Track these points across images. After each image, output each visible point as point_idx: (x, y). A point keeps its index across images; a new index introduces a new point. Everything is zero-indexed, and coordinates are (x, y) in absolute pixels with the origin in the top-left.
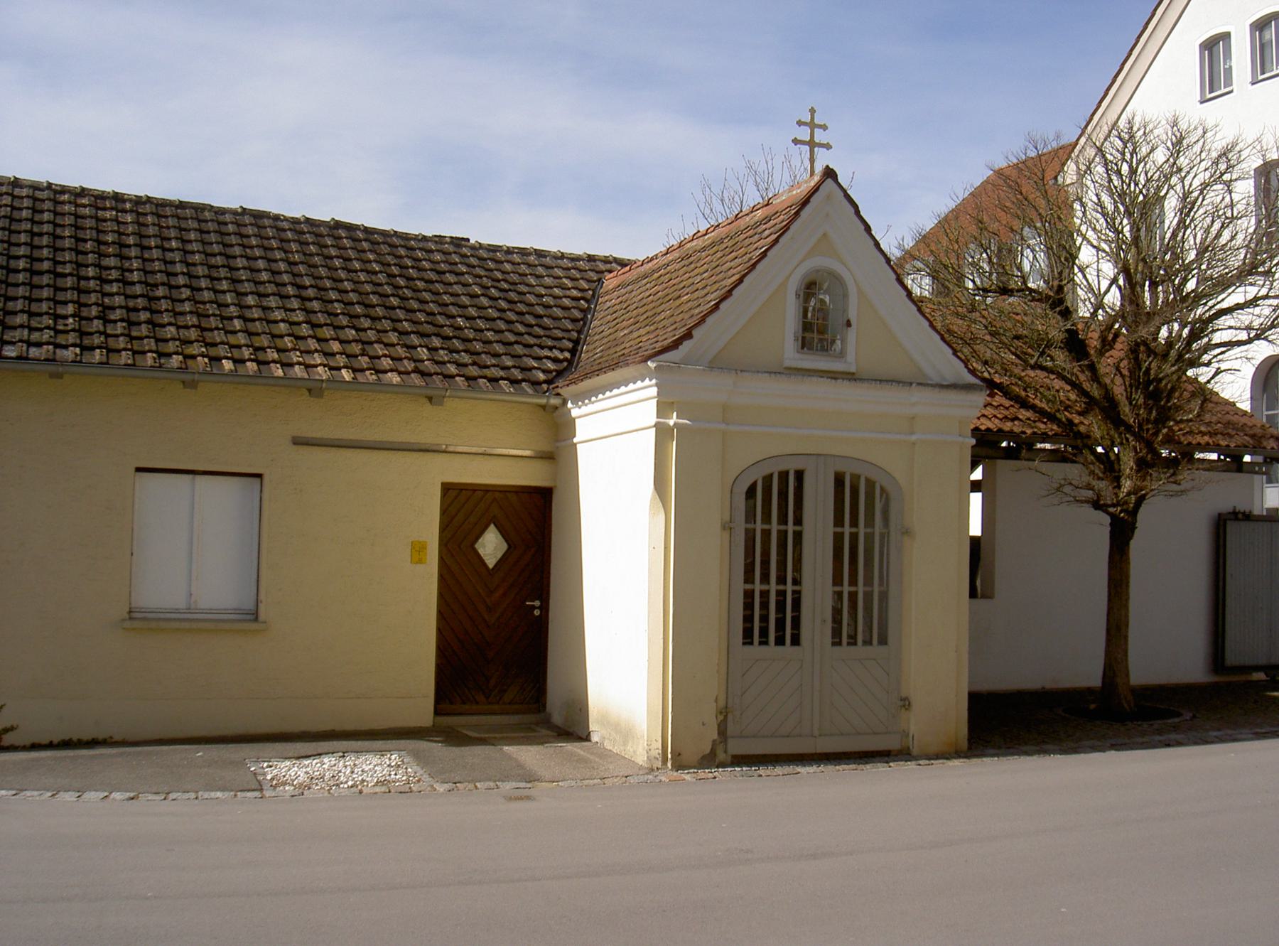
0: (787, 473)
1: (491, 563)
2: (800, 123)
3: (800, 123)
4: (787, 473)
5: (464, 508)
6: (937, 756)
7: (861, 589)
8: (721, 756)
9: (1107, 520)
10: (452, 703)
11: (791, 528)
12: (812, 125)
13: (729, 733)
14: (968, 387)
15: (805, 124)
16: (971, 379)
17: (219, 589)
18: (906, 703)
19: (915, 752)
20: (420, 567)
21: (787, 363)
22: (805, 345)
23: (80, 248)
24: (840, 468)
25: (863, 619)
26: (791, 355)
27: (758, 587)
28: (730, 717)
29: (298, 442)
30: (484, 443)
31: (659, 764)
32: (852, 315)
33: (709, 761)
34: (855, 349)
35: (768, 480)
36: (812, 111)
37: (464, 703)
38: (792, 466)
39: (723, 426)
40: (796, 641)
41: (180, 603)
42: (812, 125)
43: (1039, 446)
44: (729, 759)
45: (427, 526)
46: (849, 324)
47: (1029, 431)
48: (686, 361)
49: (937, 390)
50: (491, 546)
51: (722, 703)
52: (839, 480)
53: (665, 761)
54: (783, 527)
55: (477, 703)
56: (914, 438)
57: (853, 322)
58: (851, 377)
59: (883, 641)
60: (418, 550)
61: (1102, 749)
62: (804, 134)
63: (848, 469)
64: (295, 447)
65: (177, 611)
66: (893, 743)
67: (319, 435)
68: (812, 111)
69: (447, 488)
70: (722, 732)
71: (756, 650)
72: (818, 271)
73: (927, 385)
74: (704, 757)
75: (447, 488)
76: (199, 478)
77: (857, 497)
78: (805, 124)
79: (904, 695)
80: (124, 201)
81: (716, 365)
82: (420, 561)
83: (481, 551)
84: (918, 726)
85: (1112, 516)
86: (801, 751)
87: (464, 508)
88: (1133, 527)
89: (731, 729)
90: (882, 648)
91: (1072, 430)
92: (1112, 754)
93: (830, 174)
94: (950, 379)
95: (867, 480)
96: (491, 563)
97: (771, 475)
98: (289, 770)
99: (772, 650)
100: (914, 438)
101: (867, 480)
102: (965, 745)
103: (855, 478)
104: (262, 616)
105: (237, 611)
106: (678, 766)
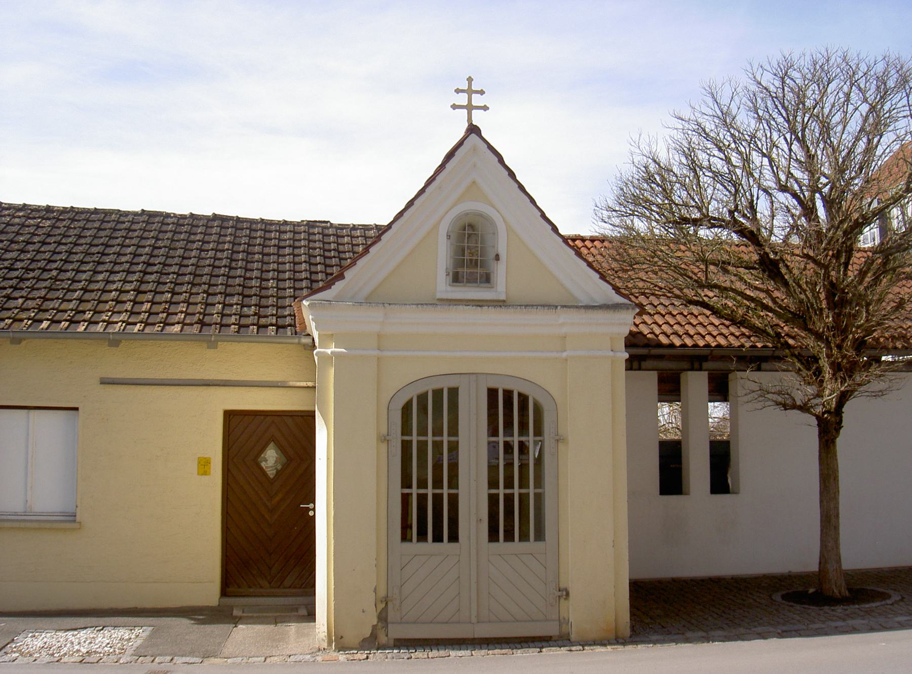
0: (441, 390)
1: (271, 473)
2: (458, 91)
3: (458, 91)
4: (441, 390)
5: (244, 432)
6: (603, 643)
7: (532, 491)
8: (383, 639)
9: (814, 421)
10: (239, 587)
11: (415, 438)
12: (470, 92)
13: (389, 619)
14: (616, 307)
15: (477, 92)
16: (619, 299)
17: (47, 498)
18: (565, 594)
19: (573, 637)
20: (205, 478)
21: (439, 296)
22: (456, 279)
23: (281, 253)
24: (493, 385)
25: (516, 516)
26: (443, 287)
27: (501, 491)
28: (390, 604)
29: (105, 382)
30: (254, 374)
31: (325, 645)
32: (502, 250)
33: (371, 643)
34: (504, 281)
35: (422, 398)
36: (470, 80)
37: (250, 587)
38: (445, 384)
39: (376, 353)
40: (454, 537)
41: (20, 508)
42: (470, 92)
43: (883, 358)
44: (392, 643)
45: (212, 444)
46: (497, 257)
47: (748, 345)
48: (339, 299)
49: (583, 311)
50: (271, 458)
51: (382, 593)
52: (492, 393)
53: (330, 644)
54: (523, 439)
55: (261, 587)
56: (565, 354)
57: (503, 256)
58: (500, 304)
59: (540, 535)
60: (204, 465)
61: (763, 636)
62: (463, 99)
63: (501, 386)
64: (102, 386)
65: (16, 514)
66: (551, 629)
67: (142, 376)
68: (470, 80)
69: (230, 416)
70: (383, 617)
71: (415, 547)
72: (467, 214)
73: (577, 307)
74: (364, 640)
75: (230, 416)
76: (32, 412)
77: (514, 412)
78: (477, 92)
79: (562, 586)
80: (53, 212)
81: (370, 301)
82: (205, 473)
83: (263, 464)
84: (577, 615)
85: (817, 417)
86: (488, 636)
87: (244, 432)
88: (839, 425)
89: (391, 615)
90: (453, 545)
91: (779, 342)
92: (774, 642)
93: (473, 130)
94: (600, 301)
95: (520, 394)
96: (271, 473)
97: (427, 393)
98: (40, 640)
99: (430, 546)
100: (565, 354)
101: (520, 394)
102: (627, 632)
103: (508, 394)
104: (78, 518)
105: (63, 514)
106: (341, 648)
